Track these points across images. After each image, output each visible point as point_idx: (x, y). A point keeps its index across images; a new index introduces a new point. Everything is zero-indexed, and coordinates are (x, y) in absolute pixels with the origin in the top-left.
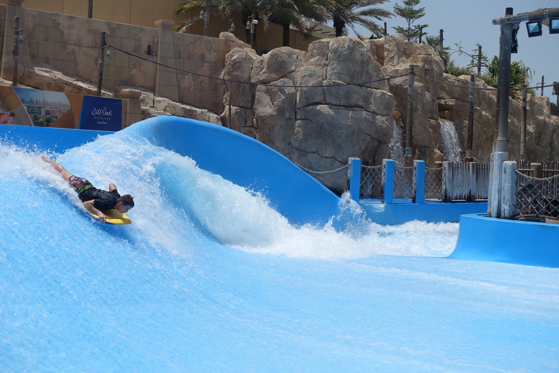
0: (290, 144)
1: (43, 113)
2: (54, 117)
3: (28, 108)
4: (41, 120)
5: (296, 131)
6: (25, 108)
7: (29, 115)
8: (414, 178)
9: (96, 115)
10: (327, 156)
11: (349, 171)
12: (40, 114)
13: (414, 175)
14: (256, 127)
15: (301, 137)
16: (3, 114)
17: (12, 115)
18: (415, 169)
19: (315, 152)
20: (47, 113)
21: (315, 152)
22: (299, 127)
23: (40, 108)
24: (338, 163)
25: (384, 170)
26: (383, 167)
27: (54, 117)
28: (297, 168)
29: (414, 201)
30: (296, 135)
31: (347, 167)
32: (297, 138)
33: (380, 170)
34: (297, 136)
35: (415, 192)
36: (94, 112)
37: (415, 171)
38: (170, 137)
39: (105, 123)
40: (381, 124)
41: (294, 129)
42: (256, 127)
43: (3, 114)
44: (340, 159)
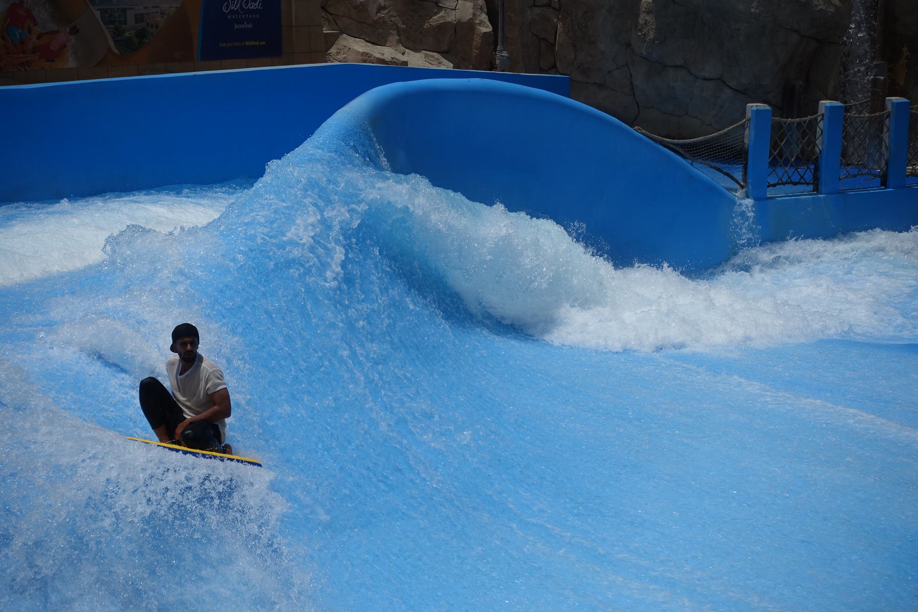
0: (628, 45)
1: (130, 16)
2: (152, 26)
3: (102, 13)
4: (127, 34)
5: (641, 21)
6: (98, 14)
7: (104, 27)
8: (886, 136)
9: (232, 12)
10: (707, 75)
11: (747, 132)
12: (126, 24)
13: (885, 129)
14: (557, 6)
15: (652, 35)
16: (58, 32)
17: (74, 31)
18: (888, 116)
19: (681, 67)
20: (139, 18)
21: (681, 67)
22: (648, 12)
23: (124, 10)
24: (729, 91)
25: (821, 124)
26: (819, 118)
27: (152, 26)
28: (640, 139)
29: (884, 183)
30: (641, 31)
31: (743, 125)
32: (644, 35)
33: (813, 125)
34: (645, 30)
35: (887, 164)
36: (227, 6)
37: (887, 121)
38: (408, 140)
39: (250, 26)
40: (823, 7)
41: (637, 16)
42: (557, 6)
43: (58, 32)
44: (733, 84)
